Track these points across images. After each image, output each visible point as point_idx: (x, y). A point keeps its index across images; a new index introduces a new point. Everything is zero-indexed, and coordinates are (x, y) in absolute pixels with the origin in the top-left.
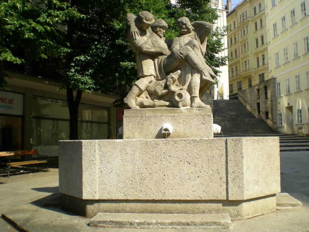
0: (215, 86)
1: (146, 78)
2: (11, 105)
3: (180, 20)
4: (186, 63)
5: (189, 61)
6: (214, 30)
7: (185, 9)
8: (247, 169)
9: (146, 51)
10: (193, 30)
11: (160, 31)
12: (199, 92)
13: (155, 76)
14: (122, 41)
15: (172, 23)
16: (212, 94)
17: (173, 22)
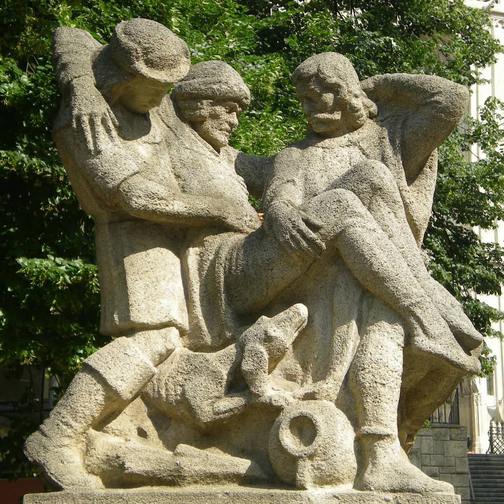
0: (481, 383)
1: (140, 336)
3: (310, 65)
4: (333, 269)
5: (349, 262)
6: (475, 114)
7: (335, 10)
9: (146, 210)
10: (371, 116)
11: (215, 116)
12: (395, 416)
13: (186, 326)
14: (31, 155)
15: (272, 79)
16: (463, 421)
17: (275, 75)
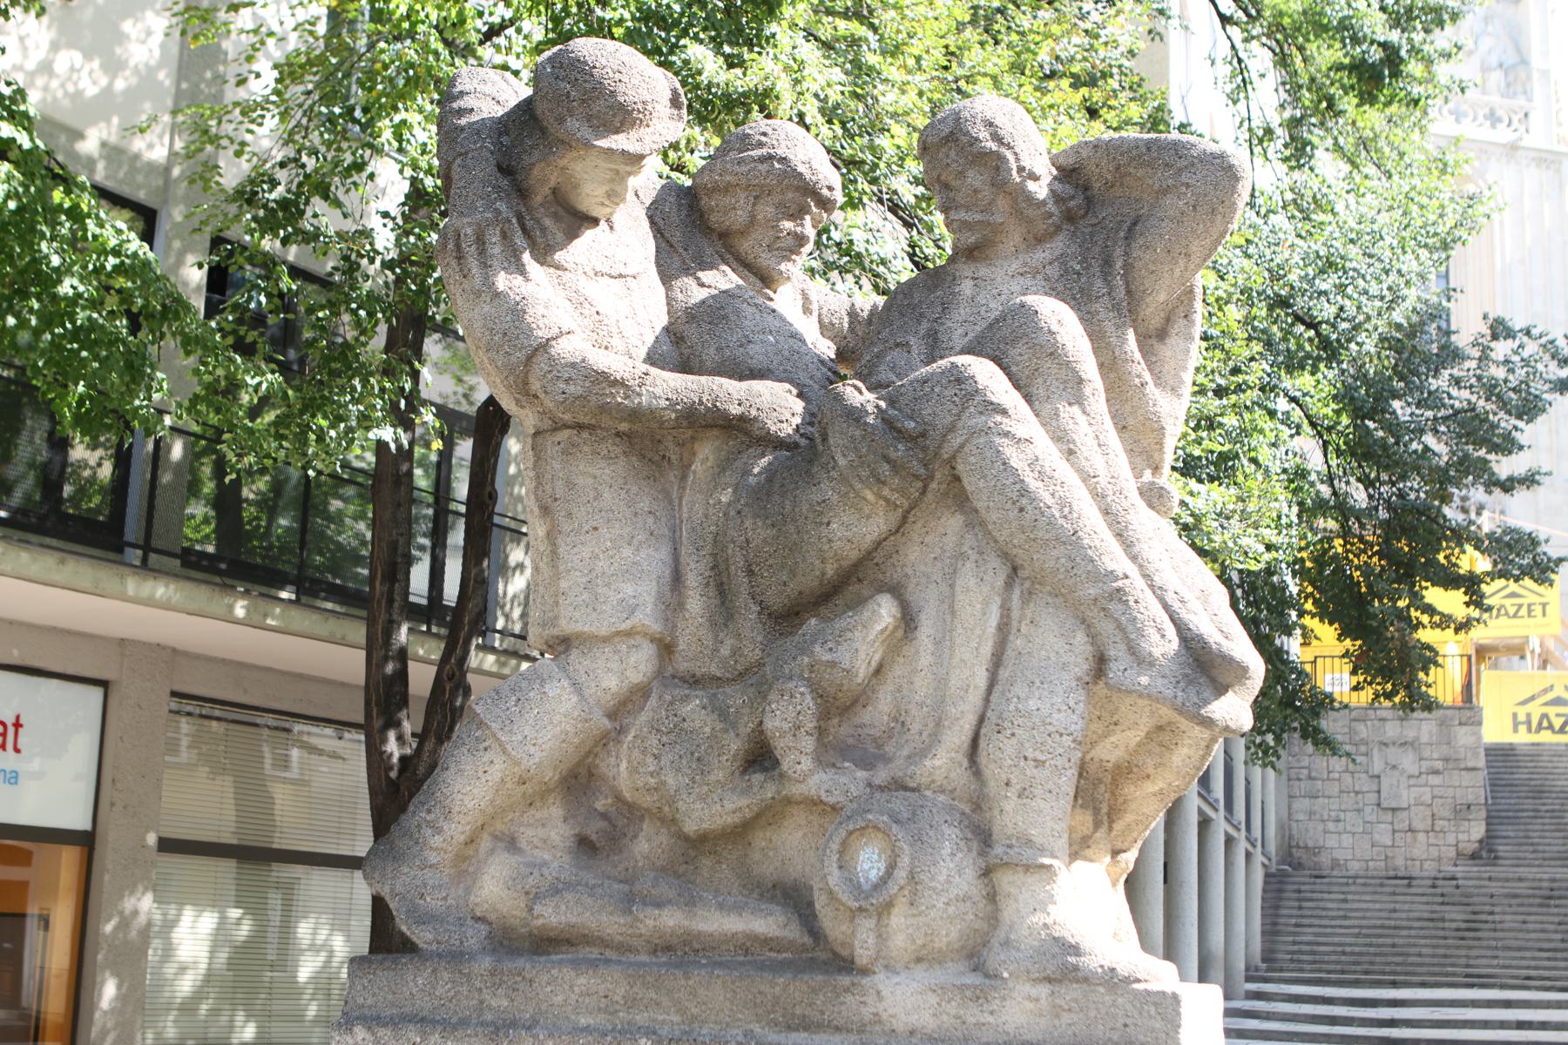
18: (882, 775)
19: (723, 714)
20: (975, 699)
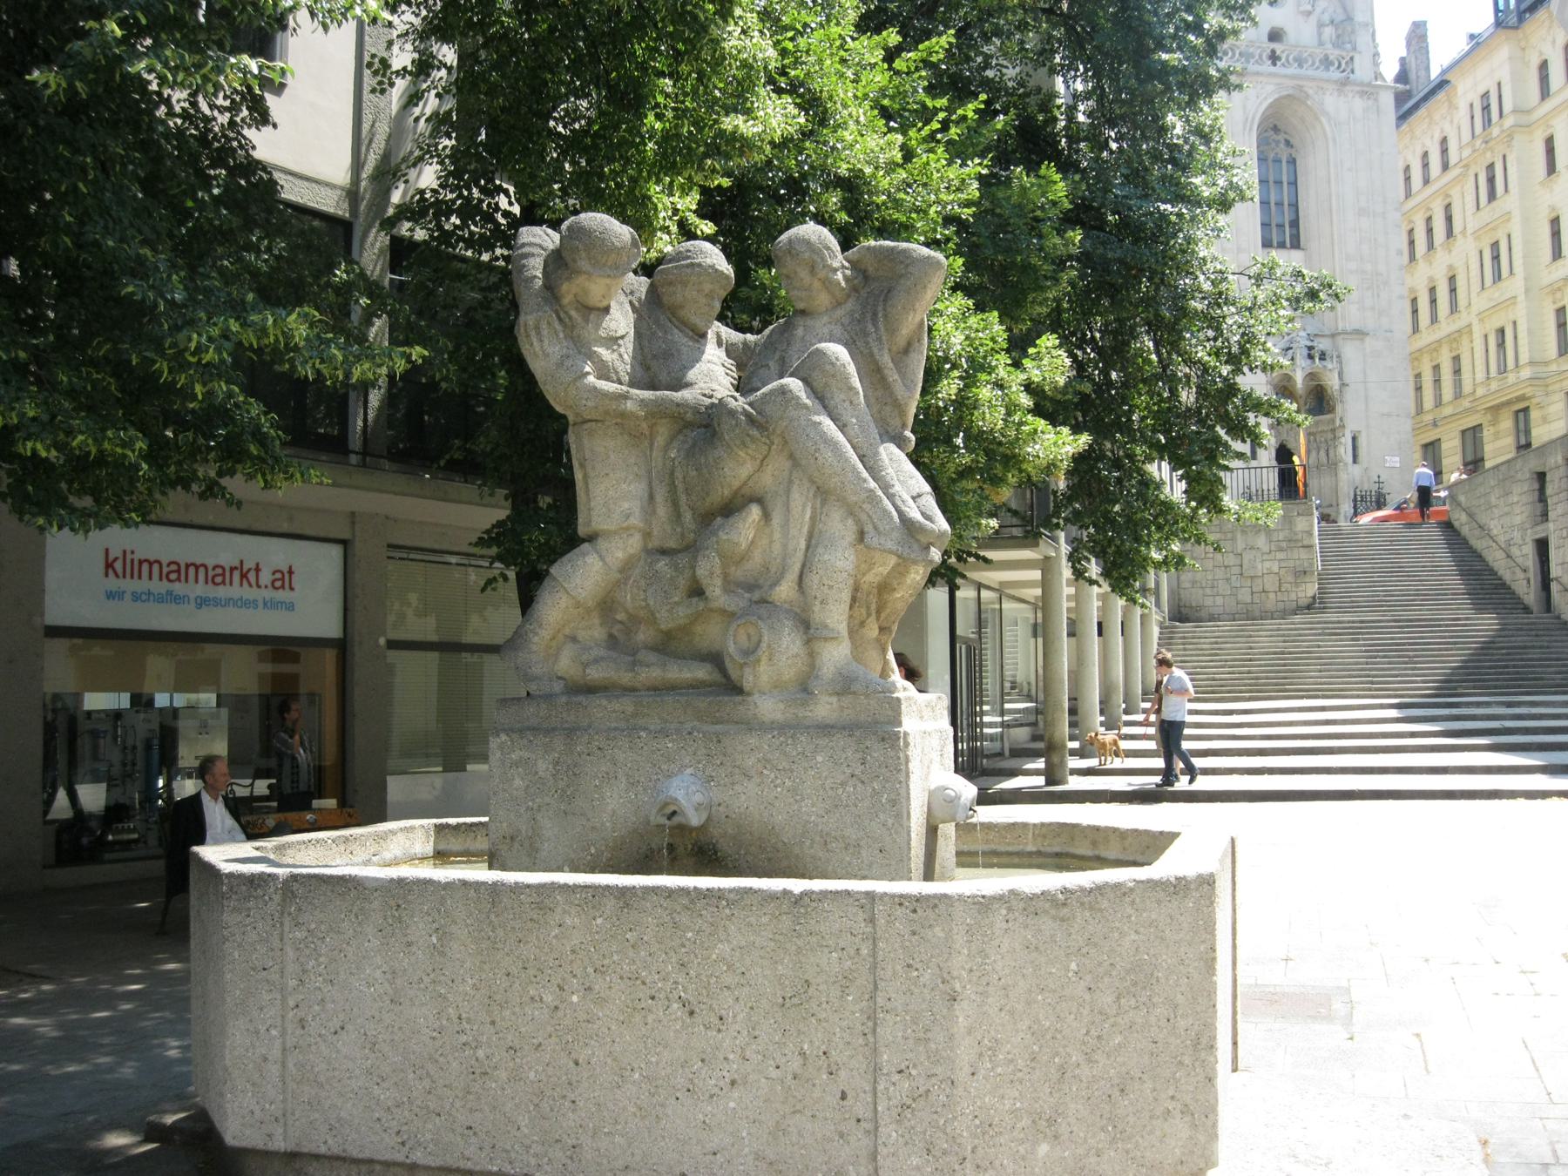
2: (281, 595)
8: (981, 1055)
18: (756, 596)
19: (676, 569)
20: (800, 555)
